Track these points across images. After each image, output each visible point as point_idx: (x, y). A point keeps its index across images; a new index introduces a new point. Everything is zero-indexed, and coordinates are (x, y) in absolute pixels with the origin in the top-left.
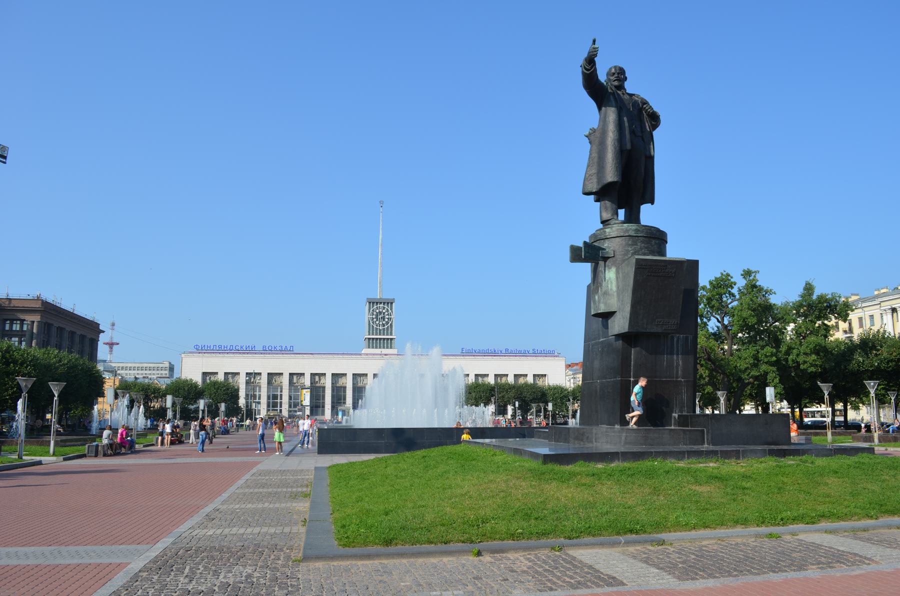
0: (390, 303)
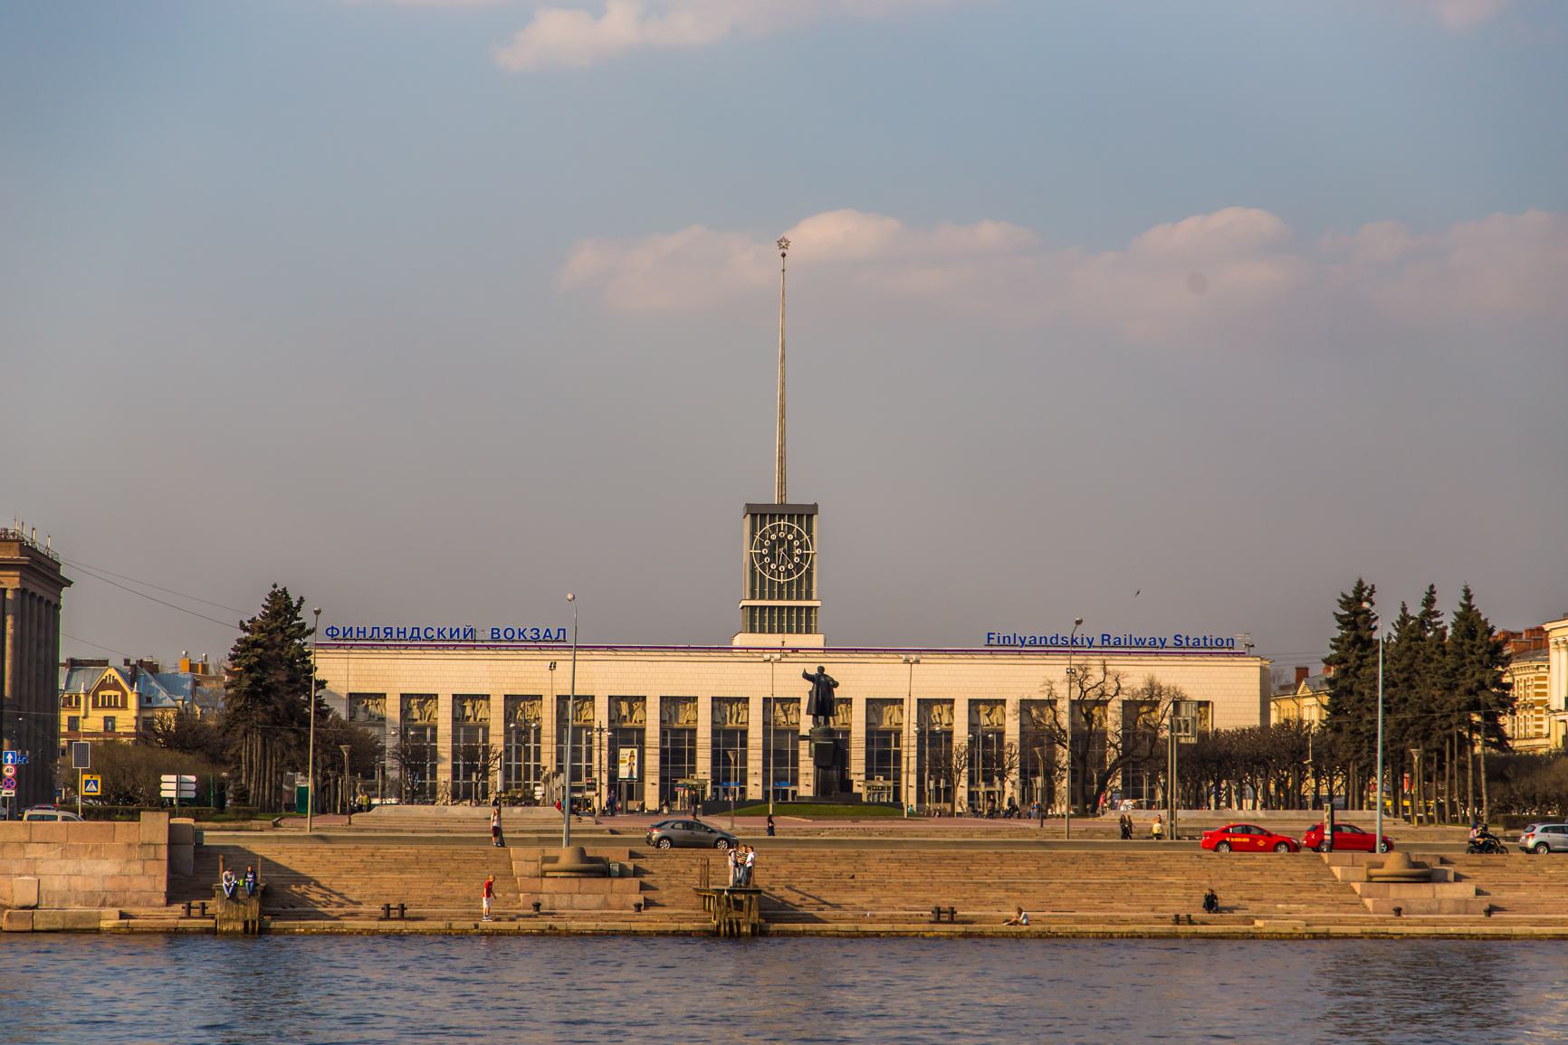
0: (805, 514)
